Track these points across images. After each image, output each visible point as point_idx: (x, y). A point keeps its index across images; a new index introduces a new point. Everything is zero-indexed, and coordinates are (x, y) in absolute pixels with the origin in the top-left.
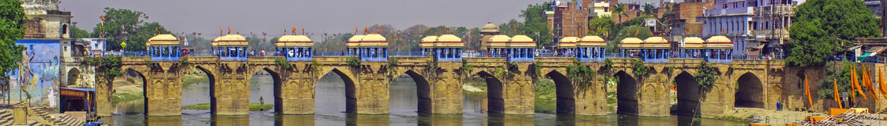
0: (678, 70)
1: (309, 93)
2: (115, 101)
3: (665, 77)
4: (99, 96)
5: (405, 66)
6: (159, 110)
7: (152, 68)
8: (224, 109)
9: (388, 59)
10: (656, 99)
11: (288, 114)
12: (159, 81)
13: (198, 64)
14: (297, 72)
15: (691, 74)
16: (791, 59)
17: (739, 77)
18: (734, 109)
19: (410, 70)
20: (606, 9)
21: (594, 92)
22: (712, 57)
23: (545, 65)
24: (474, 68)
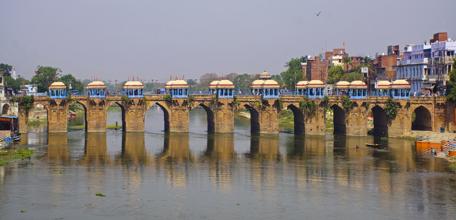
0: (373, 104)
1: (141, 118)
2: (38, 123)
3: (364, 109)
4: (20, 121)
5: (199, 101)
6: (54, 129)
7: (51, 103)
8: (92, 128)
9: (188, 96)
10: (358, 125)
11: (129, 132)
12: (54, 111)
13: (77, 100)
14: (134, 105)
15: (382, 107)
16: (450, 96)
17: (415, 109)
18: (411, 132)
19: (201, 103)
20: (340, 61)
21: (317, 119)
22: (396, 95)
23: (285, 100)
24: (241, 102)
